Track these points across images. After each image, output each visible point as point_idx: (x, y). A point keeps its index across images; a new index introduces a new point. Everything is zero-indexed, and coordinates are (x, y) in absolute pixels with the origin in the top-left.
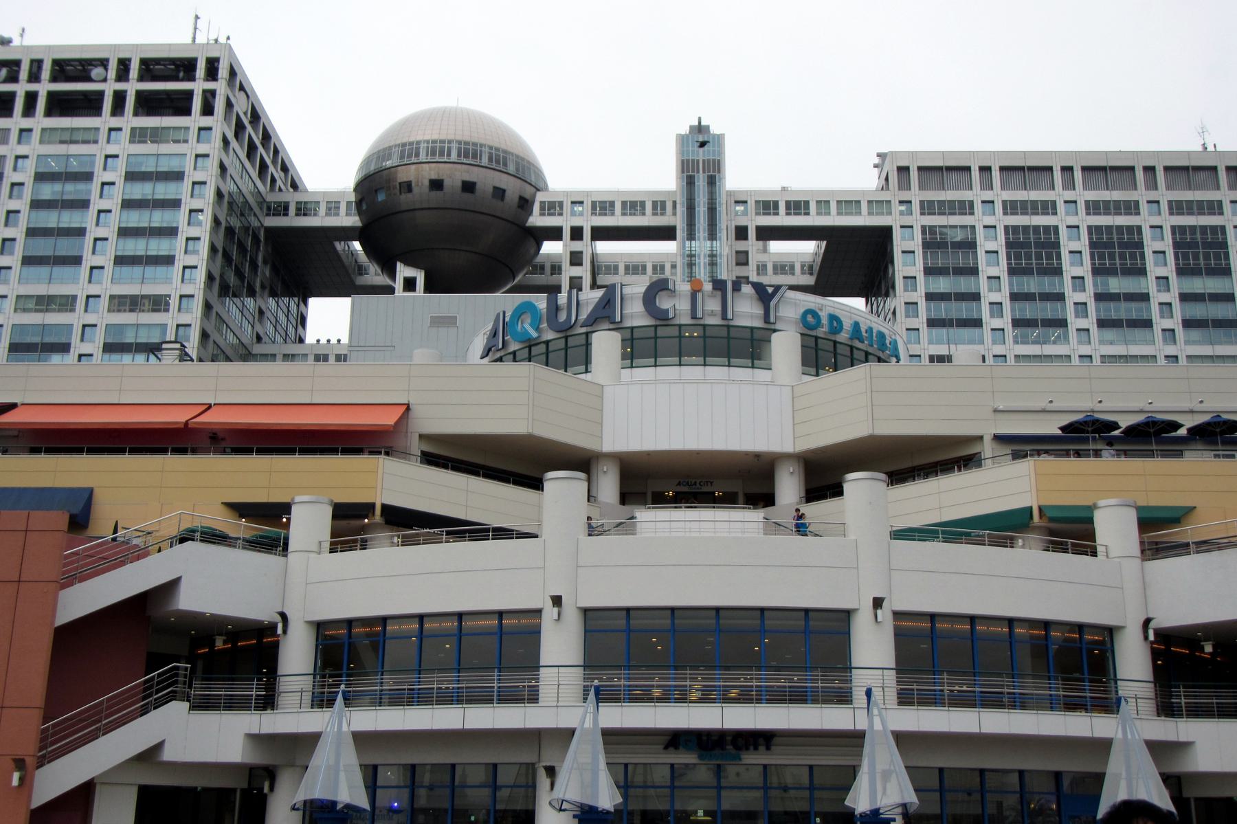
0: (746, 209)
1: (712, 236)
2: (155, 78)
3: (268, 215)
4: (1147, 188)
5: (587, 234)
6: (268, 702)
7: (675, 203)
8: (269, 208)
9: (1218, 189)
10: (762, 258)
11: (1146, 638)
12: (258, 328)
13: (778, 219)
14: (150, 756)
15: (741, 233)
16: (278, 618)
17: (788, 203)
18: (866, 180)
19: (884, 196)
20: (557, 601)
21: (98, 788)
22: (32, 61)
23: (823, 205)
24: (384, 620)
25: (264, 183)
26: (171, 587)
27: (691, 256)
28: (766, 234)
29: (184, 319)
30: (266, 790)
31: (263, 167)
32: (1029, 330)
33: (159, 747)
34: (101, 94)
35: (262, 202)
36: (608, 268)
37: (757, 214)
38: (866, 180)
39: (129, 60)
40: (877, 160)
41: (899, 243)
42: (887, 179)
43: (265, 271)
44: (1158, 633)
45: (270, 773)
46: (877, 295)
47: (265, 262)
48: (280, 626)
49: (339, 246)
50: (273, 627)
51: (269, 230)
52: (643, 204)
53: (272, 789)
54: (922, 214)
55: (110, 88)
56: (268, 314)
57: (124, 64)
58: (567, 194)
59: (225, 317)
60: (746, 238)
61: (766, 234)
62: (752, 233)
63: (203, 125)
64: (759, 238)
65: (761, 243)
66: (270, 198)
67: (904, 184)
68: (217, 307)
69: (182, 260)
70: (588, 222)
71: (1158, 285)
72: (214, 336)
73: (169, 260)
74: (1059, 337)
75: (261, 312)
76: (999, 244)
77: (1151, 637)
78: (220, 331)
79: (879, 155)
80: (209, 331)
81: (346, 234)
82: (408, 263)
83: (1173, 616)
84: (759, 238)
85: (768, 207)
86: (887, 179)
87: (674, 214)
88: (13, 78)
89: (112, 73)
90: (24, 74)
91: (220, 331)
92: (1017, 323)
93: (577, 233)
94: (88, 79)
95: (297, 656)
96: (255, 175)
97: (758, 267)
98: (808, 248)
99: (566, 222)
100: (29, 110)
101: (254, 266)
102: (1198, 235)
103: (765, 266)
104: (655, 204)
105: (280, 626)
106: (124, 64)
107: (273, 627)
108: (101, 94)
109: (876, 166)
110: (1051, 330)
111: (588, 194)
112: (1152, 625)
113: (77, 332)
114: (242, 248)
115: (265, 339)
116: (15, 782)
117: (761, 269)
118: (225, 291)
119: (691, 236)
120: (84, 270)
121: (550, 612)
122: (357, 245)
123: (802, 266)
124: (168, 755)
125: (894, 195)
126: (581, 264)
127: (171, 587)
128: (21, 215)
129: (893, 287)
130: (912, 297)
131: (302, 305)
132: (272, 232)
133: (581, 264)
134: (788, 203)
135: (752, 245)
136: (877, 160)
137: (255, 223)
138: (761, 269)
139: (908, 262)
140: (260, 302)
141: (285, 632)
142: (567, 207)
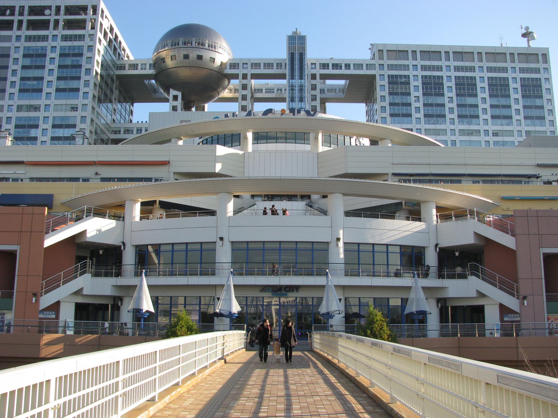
0: (315, 67)
1: (301, 78)
2: (71, 14)
3: (117, 70)
4: (479, 61)
5: (249, 76)
6: (118, 274)
7: (286, 64)
8: (118, 67)
9: (506, 62)
10: (323, 86)
11: (436, 251)
12: (114, 117)
13: (332, 69)
14: (78, 292)
15: (314, 77)
16: (122, 244)
17: (333, 65)
18: (365, 55)
19: (373, 62)
20: (221, 239)
21: (61, 303)
22: (20, 7)
23: (348, 66)
24: (160, 245)
25: (116, 57)
26: (84, 232)
27: (292, 86)
28: (324, 77)
29: (84, 114)
30: (120, 305)
31: (115, 49)
32: (431, 119)
33: (81, 289)
34: (49, 21)
35: (115, 65)
36: (258, 90)
37: (320, 69)
38: (365, 55)
39: (60, 6)
40: (370, 47)
41: (379, 82)
42: (374, 55)
43: (116, 93)
44: (440, 248)
45: (121, 299)
46: (370, 102)
47: (116, 89)
48: (122, 247)
49: (146, 82)
50: (120, 247)
51: (117, 76)
52: (272, 64)
53: (121, 304)
54: (388, 70)
55: (52, 18)
56: (117, 111)
57: (58, 8)
58: (241, 60)
59: (100, 113)
60: (315, 79)
61: (324, 77)
62: (318, 77)
63: (90, 33)
64: (321, 79)
65: (322, 81)
66: (118, 62)
67: (381, 58)
68: (97, 109)
69: (83, 89)
70: (250, 71)
71: (482, 101)
72: (96, 121)
73: (77, 90)
74: (442, 121)
75: (115, 110)
76: (419, 83)
77: (438, 251)
78: (98, 119)
79: (371, 45)
80: (94, 119)
81: (149, 77)
82: (175, 89)
83: (446, 243)
84: (321, 79)
85: (325, 66)
86: (374, 55)
87: (286, 68)
88: (12, 14)
89: (53, 12)
90: (17, 12)
91: (98, 119)
92: (426, 116)
93: (245, 76)
94: (44, 14)
95: (129, 258)
96: (111, 53)
97: (321, 90)
98: (342, 82)
99: (240, 72)
100: (20, 27)
101: (112, 91)
102: (498, 81)
103: (324, 90)
104: (277, 64)
105: (122, 247)
106: (58, 8)
107: (120, 247)
108: (49, 21)
109: (370, 49)
110: (439, 119)
111: (249, 60)
112: (439, 246)
113: (41, 119)
114: (107, 84)
115: (116, 121)
116: (34, 301)
117: (322, 91)
118: (100, 101)
119: (292, 77)
120: (44, 94)
121: (219, 243)
122: (153, 81)
123: (340, 90)
124: (85, 292)
125: (377, 62)
126: (247, 89)
127: (84, 232)
128: (18, 72)
129: (376, 100)
130: (383, 104)
131: (131, 106)
132: (118, 76)
133: (247, 89)
134: (333, 65)
135: (318, 82)
136: (370, 47)
137: (112, 73)
138: (322, 91)
139: (382, 89)
140: (114, 106)
141: (124, 249)
142: (241, 65)
